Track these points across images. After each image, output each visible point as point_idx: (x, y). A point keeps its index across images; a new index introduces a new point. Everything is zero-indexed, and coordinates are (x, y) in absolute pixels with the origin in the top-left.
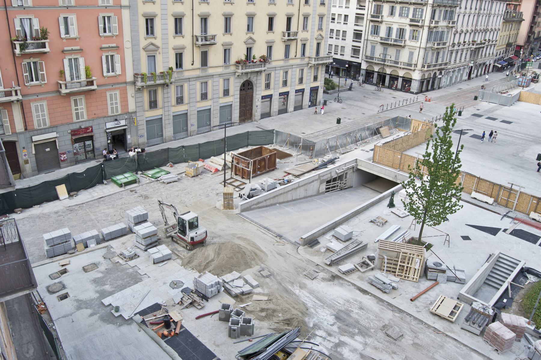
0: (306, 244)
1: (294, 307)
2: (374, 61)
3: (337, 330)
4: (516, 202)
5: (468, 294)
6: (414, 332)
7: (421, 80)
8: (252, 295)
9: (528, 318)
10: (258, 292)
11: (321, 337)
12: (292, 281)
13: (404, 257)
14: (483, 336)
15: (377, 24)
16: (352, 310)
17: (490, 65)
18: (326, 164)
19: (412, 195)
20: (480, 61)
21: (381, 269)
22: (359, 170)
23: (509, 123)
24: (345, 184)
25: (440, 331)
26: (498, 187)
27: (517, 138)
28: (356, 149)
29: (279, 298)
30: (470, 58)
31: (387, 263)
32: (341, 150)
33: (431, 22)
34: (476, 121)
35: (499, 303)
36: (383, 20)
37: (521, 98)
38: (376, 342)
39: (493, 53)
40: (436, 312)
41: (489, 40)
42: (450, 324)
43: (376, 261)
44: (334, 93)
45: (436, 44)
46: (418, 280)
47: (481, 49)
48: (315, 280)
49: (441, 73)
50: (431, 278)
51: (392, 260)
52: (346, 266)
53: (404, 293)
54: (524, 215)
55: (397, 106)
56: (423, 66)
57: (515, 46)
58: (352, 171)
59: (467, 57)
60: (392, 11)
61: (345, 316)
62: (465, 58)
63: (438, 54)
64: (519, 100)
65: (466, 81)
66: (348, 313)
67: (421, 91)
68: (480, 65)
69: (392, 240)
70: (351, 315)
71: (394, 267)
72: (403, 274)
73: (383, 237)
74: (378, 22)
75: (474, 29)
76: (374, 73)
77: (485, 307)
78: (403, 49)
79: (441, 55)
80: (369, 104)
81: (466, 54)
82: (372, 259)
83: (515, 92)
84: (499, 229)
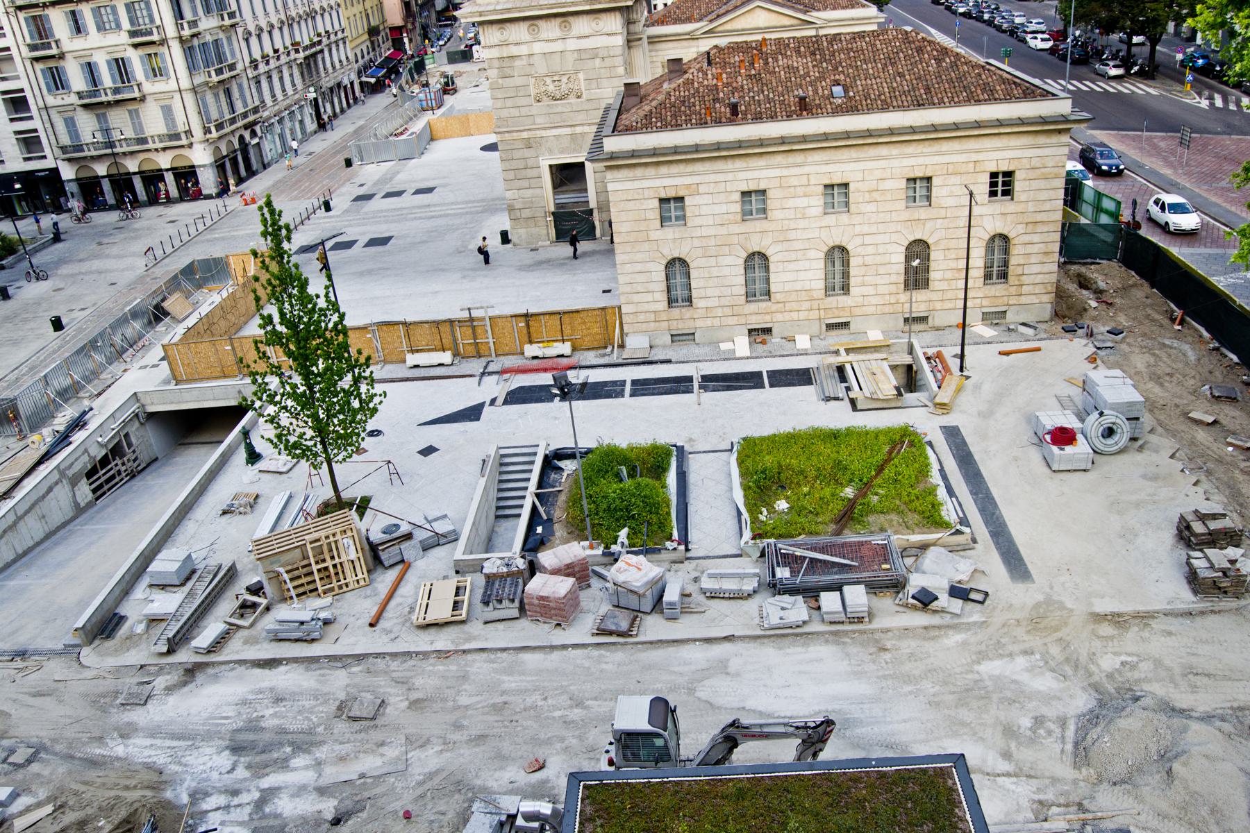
0: (94, 638)
1: (127, 788)
2: (87, 153)
3: (247, 774)
4: (491, 340)
5: (471, 553)
6: (403, 683)
7: (216, 161)
8: (9, 823)
9: (587, 539)
10: (21, 808)
11: (218, 809)
12: (97, 733)
13: (318, 550)
14: (526, 615)
15: (52, 64)
16: (261, 714)
17: (352, 83)
18: (67, 436)
19: (277, 415)
20: (327, 82)
21: (285, 599)
22: (152, 416)
23: (430, 190)
24: (134, 461)
25: (449, 652)
26: (447, 326)
27: (454, 215)
28: (125, 371)
29: (82, 788)
30: (304, 81)
31: (291, 580)
32: (92, 389)
33: (180, 27)
34: (365, 210)
35: (531, 539)
36: (65, 49)
37: (434, 133)
38: (337, 747)
39: (347, 58)
40: (427, 621)
41: (327, 32)
42: (461, 626)
43: (268, 589)
44: (20, 261)
45: (213, 73)
46: (367, 579)
47: (319, 57)
48: (150, 702)
49: (254, 134)
50: (392, 562)
51: (298, 569)
52: (204, 638)
53: (352, 619)
54: (515, 357)
55: (185, 238)
56: (207, 131)
57: (388, 31)
58: (137, 424)
59: (296, 82)
60: (76, 22)
61: (251, 737)
62: (294, 85)
63: (228, 93)
64: (432, 139)
65: (315, 132)
66: (253, 726)
67: (224, 191)
68: (331, 89)
69: (285, 525)
70: (263, 725)
71: (309, 579)
72: (335, 584)
73: (263, 530)
74: (53, 57)
75: (283, 17)
76: (100, 182)
77: (506, 560)
78: (143, 105)
79: (236, 93)
80: (119, 257)
81: (291, 75)
82: (256, 590)
83: (418, 126)
84: (482, 405)
